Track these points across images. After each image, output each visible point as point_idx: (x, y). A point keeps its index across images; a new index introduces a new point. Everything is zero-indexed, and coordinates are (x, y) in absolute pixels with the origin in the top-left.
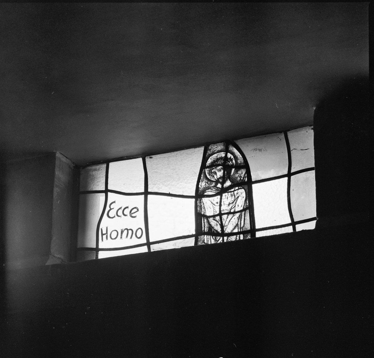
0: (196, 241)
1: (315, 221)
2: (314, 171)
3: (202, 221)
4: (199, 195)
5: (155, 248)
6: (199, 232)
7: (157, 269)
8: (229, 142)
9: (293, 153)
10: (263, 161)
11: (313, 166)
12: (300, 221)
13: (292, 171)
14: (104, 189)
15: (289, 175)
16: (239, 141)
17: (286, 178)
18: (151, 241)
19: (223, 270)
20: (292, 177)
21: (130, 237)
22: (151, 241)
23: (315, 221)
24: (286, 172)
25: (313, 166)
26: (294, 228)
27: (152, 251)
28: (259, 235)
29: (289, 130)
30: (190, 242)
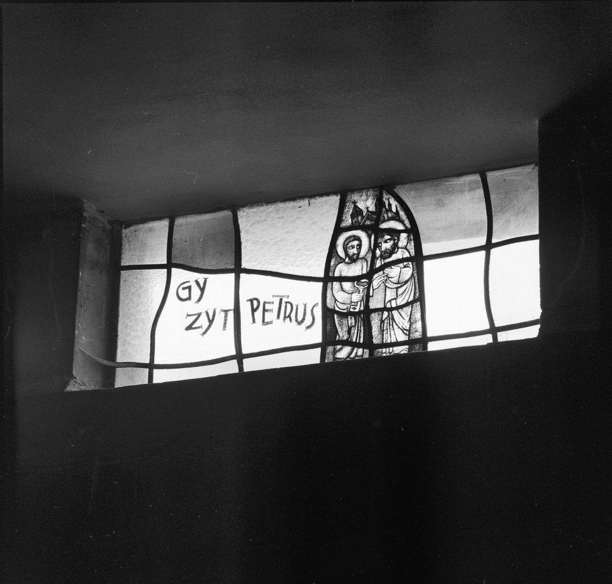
0: (323, 356)
1: (538, 326)
2: (537, 242)
3: (334, 319)
4: (328, 279)
5: (250, 365)
6: (330, 339)
7: (245, 405)
8: (384, 187)
9: (493, 197)
10: (448, 215)
11: (537, 232)
12: (487, 215)
13: (494, 241)
14: (165, 262)
15: (488, 247)
16: (398, 187)
17: (483, 253)
18: (244, 352)
19: (369, 411)
20: (494, 251)
21: (271, 305)
22: (245, 351)
23: (538, 326)
24: (482, 241)
25: (537, 232)
26: (495, 338)
27: (246, 370)
28: (432, 347)
29: (243, 206)
30: (313, 357)
